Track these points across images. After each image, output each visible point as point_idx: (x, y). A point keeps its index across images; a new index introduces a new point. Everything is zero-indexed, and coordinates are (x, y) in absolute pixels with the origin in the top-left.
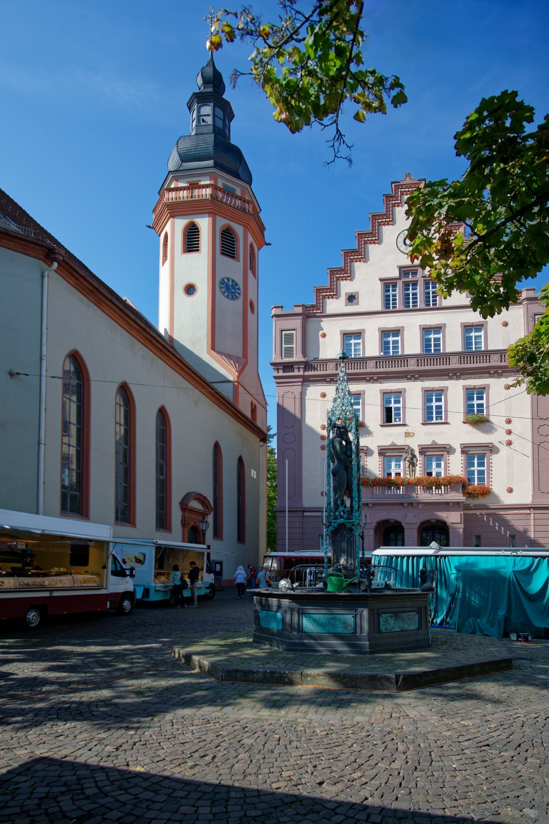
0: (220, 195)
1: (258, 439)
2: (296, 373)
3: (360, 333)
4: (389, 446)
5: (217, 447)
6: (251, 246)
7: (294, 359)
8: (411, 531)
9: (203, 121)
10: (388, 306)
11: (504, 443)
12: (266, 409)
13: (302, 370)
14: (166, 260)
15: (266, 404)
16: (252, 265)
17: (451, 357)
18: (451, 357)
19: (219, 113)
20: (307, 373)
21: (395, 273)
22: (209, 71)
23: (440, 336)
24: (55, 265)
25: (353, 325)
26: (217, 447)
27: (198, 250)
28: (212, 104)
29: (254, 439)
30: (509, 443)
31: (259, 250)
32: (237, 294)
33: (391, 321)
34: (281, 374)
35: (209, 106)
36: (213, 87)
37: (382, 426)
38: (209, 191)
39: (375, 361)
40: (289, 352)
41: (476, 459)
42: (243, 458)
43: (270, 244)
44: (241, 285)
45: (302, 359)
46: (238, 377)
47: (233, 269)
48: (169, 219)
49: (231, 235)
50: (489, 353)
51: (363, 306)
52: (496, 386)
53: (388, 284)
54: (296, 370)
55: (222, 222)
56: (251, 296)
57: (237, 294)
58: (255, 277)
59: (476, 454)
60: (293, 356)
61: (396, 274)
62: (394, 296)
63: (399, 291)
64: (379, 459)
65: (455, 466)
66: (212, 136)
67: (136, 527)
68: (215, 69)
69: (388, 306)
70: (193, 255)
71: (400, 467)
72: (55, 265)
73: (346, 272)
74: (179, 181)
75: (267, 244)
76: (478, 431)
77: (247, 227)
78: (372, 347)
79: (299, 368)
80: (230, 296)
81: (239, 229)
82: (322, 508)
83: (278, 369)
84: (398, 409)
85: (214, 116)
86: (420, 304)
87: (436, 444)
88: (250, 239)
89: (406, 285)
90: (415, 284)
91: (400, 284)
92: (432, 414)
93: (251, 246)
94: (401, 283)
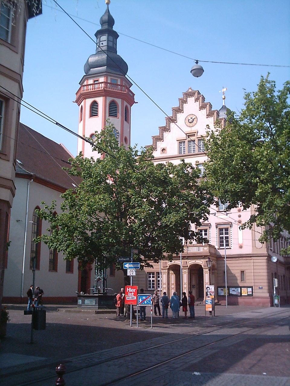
6: (126, 107)
8: (165, 271)
9: (102, 44)
16: (127, 117)
19: (111, 38)
21: (184, 136)
22: (106, 18)
24: (32, 180)
27: (97, 115)
28: (107, 35)
32: (117, 136)
35: (105, 36)
36: (108, 25)
44: (119, 131)
55: (109, 99)
57: (117, 136)
62: (184, 148)
67: (57, 272)
70: (94, 119)
72: (32, 180)
73: (159, 139)
74: (89, 79)
75: (136, 103)
76: (66, 296)
81: (119, 101)
85: (108, 41)
88: (125, 103)
91: (186, 142)
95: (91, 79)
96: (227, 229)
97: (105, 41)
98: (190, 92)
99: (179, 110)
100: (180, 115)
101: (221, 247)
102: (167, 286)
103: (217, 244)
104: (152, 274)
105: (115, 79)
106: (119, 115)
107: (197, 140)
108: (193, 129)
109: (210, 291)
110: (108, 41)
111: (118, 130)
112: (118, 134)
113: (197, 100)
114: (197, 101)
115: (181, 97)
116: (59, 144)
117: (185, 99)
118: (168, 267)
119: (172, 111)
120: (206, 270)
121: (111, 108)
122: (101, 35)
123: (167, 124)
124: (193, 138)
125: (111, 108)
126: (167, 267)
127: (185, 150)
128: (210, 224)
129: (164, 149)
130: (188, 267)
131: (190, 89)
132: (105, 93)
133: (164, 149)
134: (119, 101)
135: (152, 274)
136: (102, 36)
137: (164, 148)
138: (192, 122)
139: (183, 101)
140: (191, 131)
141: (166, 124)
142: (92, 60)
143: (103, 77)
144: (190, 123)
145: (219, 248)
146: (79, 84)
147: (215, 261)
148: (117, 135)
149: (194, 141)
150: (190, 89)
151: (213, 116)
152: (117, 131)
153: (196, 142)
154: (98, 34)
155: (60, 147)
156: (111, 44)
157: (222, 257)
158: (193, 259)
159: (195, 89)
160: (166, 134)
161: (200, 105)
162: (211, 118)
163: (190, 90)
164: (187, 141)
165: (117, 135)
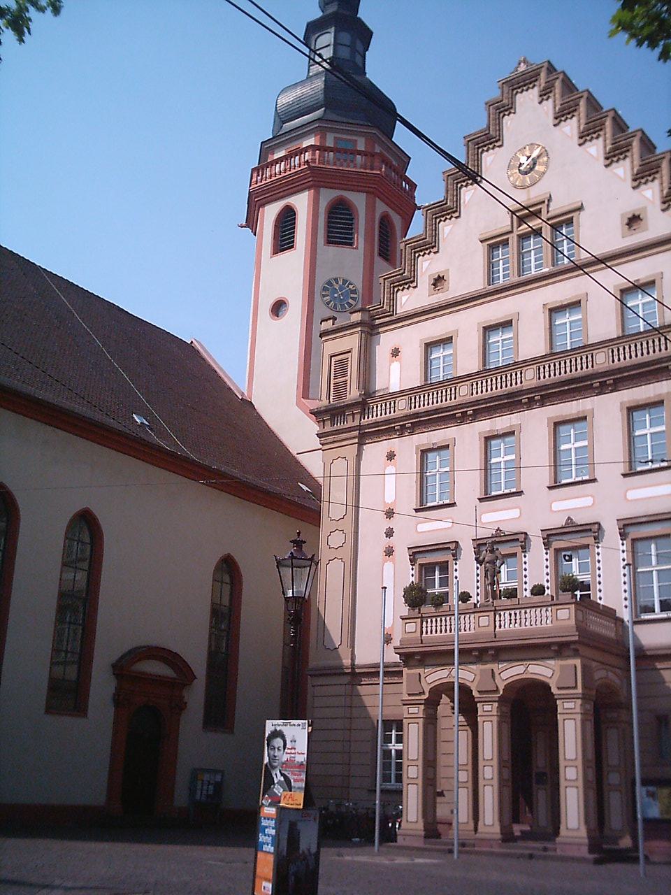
6: (385, 220)
13: (357, 417)
17: (594, 352)
19: (346, 38)
20: (365, 421)
21: (503, 221)
27: (292, 247)
32: (350, 301)
34: (328, 428)
41: (437, 573)
47: (349, 263)
49: (347, 210)
51: (455, 289)
53: (494, 244)
55: (328, 195)
57: (350, 301)
79: (353, 414)
80: (339, 307)
81: (358, 200)
83: (324, 421)
88: (381, 208)
91: (513, 239)
95: (281, 149)
97: (329, 48)
98: (523, 73)
99: (488, 139)
100: (492, 157)
102: (421, 770)
103: (627, 603)
104: (394, 727)
105: (350, 140)
106: (360, 239)
108: (535, 194)
109: (285, 758)
110: (336, 44)
111: (352, 281)
112: (355, 296)
113: (545, 94)
114: (545, 97)
115: (495, 94)
116: (189, 342)
117: (505, 101)
118: (427, 696)
119: (465, 148)
120: (566, 705)
121: (333, 223)
122: (317, 35)
123: (447, 191)
124: (535, 223)
125: (333, 223)
126: (423, 693)
128: (599, 524)
129: (439, 276)
130: (497, 690)
131: (522, 64)
132: (314, 179)
133: (439, 276)
134: (358, 200)
135: (394, 727)
136: (319, 36)
137: (441, 275)
138: (531, 169)
139: (502, 109)
140: (529, 199)
141: (444, 194)
142: (285, 100)
143: (313, 135)
144: (526, 173)
145: (637, 617)
146: (351, 244)
147: (619, 671)
148: (351, 298)
149: (537, 233)
150: (522, 64)
151: (601, 133)
152: (351, 287)
153: (547, 232)
154: (314, 28)
155: (190, 351)
156: (345, 53)
157: (648, 653)
158: (518, 660)
159: (538, 59)
160: (446, 228)
161: (555, 108)
162: (594, 141)
163: (523, 68)
164: (516, 237)
165: (351, 298)
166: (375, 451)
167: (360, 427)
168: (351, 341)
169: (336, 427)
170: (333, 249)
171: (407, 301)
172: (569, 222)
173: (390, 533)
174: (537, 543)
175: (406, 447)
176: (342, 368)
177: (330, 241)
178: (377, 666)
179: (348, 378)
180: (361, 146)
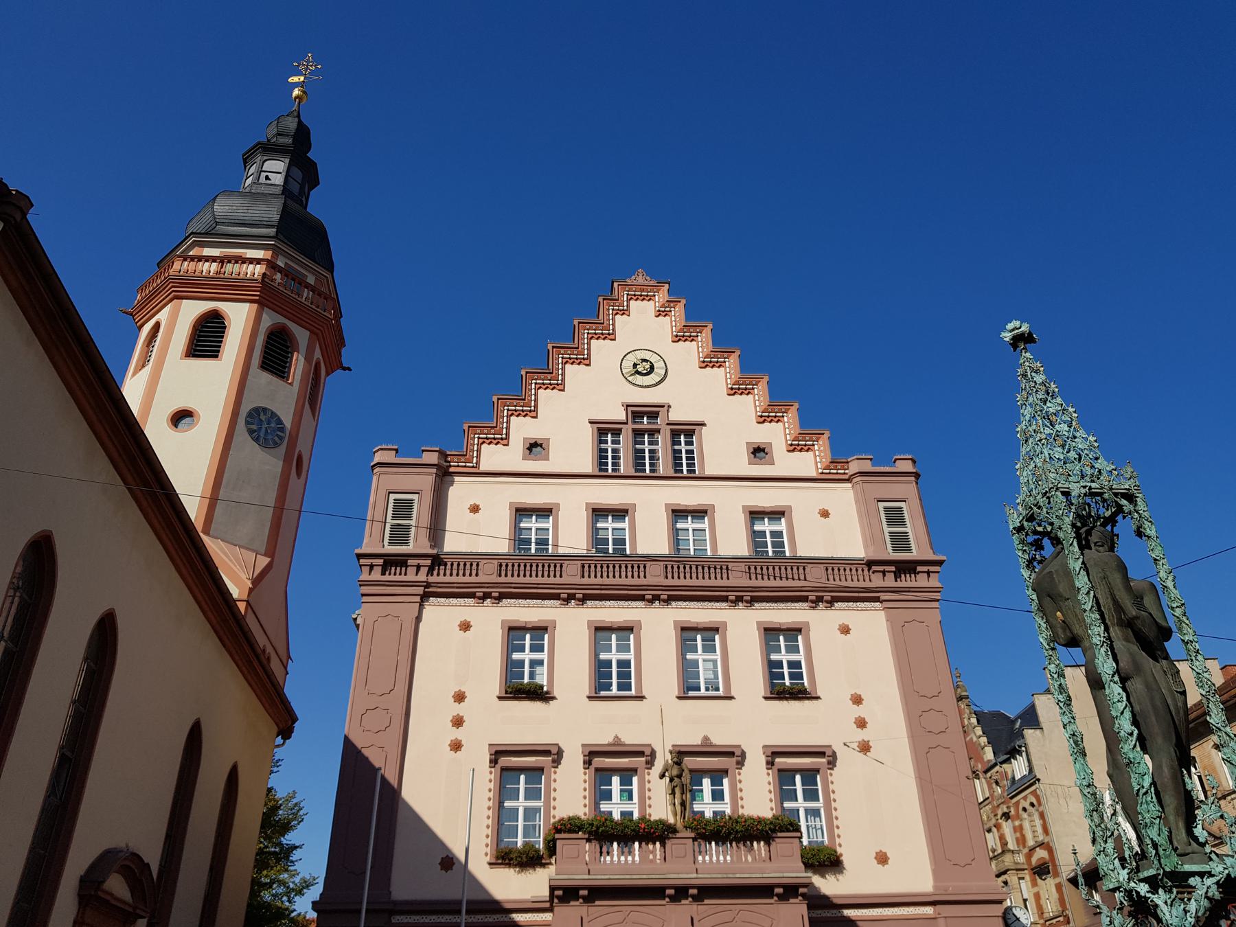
0: (278, 276)
1: (275, 729)
2: (411, 576)
3: (626, 511)
4: (609, 745)
5: (195, 737)
6: (317, 365)
7: (409, 548)
9: (267, 178)
10: (603, 468)
11: (855, 746)
12: (286, 668)
13: (424, 570)
14: (143, 366)
15: (289, 657)
18: (648, 564)
19: (298, 174)
20: (431, 579)
21: (621, 415)
23: (625, 524)
25: (535, 493)
26: (195, 737)
27: (217, 356)
28: (287, 161)
29: (266, 725)
30: (865, 748)
31: (328, 374)
33: (611, 493)
37: (766, 698)
38: (259, 270)
39: (579, 563)
40: (400, 534)
42: (240, 769)
43: (349, 369)
45: (430, 551)
46: (251, 590)
48: (171, 300)
50: (803, 563)
52: (821, 623)
53: (604, 430)
54: (411, 570)
55: (269, 319)
56: (302, 446)
58: (314, 415)
59: (800, 769)
60: (406, 543)
61: (621, 415)
63: (625, 443)
64: (583, 777)
65: (755, 795)
66: (280, 201)
68: (300, 122)
69: (603, 468)
71: (631, 798)
75: (345, 369)
77: (317, 335)
78: (572, 536)
79: (418, 567)
81: (301, 336)
82: (460, 902)
84: (624, 664)
86: (663, 467)
87: (711, 745)
88: (318, 354)
89: (638, 433)
90: (653, 433)
92: (609, 681)
93: (317, 365)
94: (630, 432)
96: (810, 776)
101: (603, 693)
107: (669, 433)
127: (693, 459)
134: (301, 336)
166: (440, 617)
167: (428, 585)
168: (426, 481)
169: (386, 578)
170: (266, 377)
171: (491, 457)
172: (689, 434)
173: (458, 722)
174: (756, 764)
175: (490, 620)
176: (403, 509)
177: (266, 365)
178: (460, 902)
179: (413, 522)
180: (311, 280)
